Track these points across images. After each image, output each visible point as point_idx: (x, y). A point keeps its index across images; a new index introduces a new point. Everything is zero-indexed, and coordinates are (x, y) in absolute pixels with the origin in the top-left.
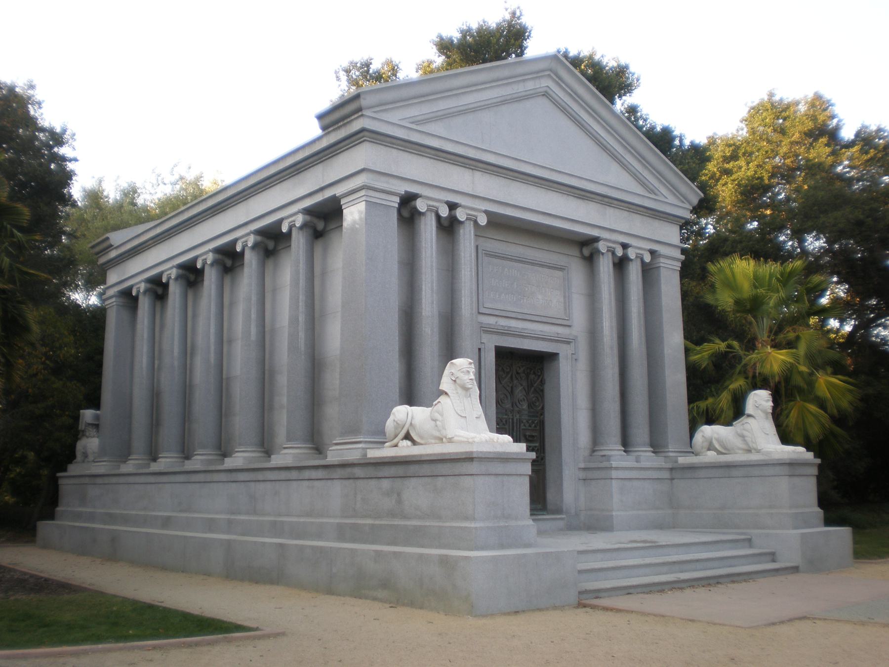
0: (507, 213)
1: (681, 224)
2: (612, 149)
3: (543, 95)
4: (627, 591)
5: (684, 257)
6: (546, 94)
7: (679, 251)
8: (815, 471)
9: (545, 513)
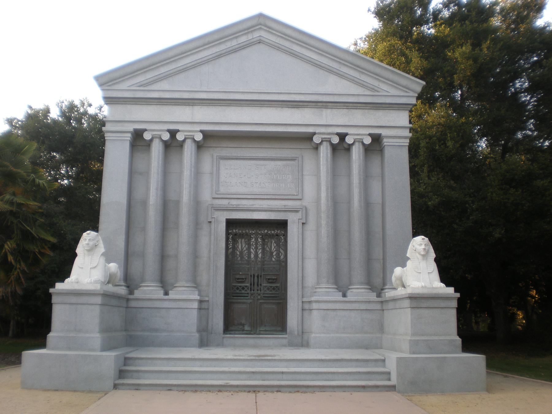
0: (223, 129)
1: (410, 109)
2: (327, 67)
3: (260, 42)
4: (169, 388)
5: (411, 134)
6: (261, 41)
7: (408, 131)
8: (455, 304)
9: (283, 333)
